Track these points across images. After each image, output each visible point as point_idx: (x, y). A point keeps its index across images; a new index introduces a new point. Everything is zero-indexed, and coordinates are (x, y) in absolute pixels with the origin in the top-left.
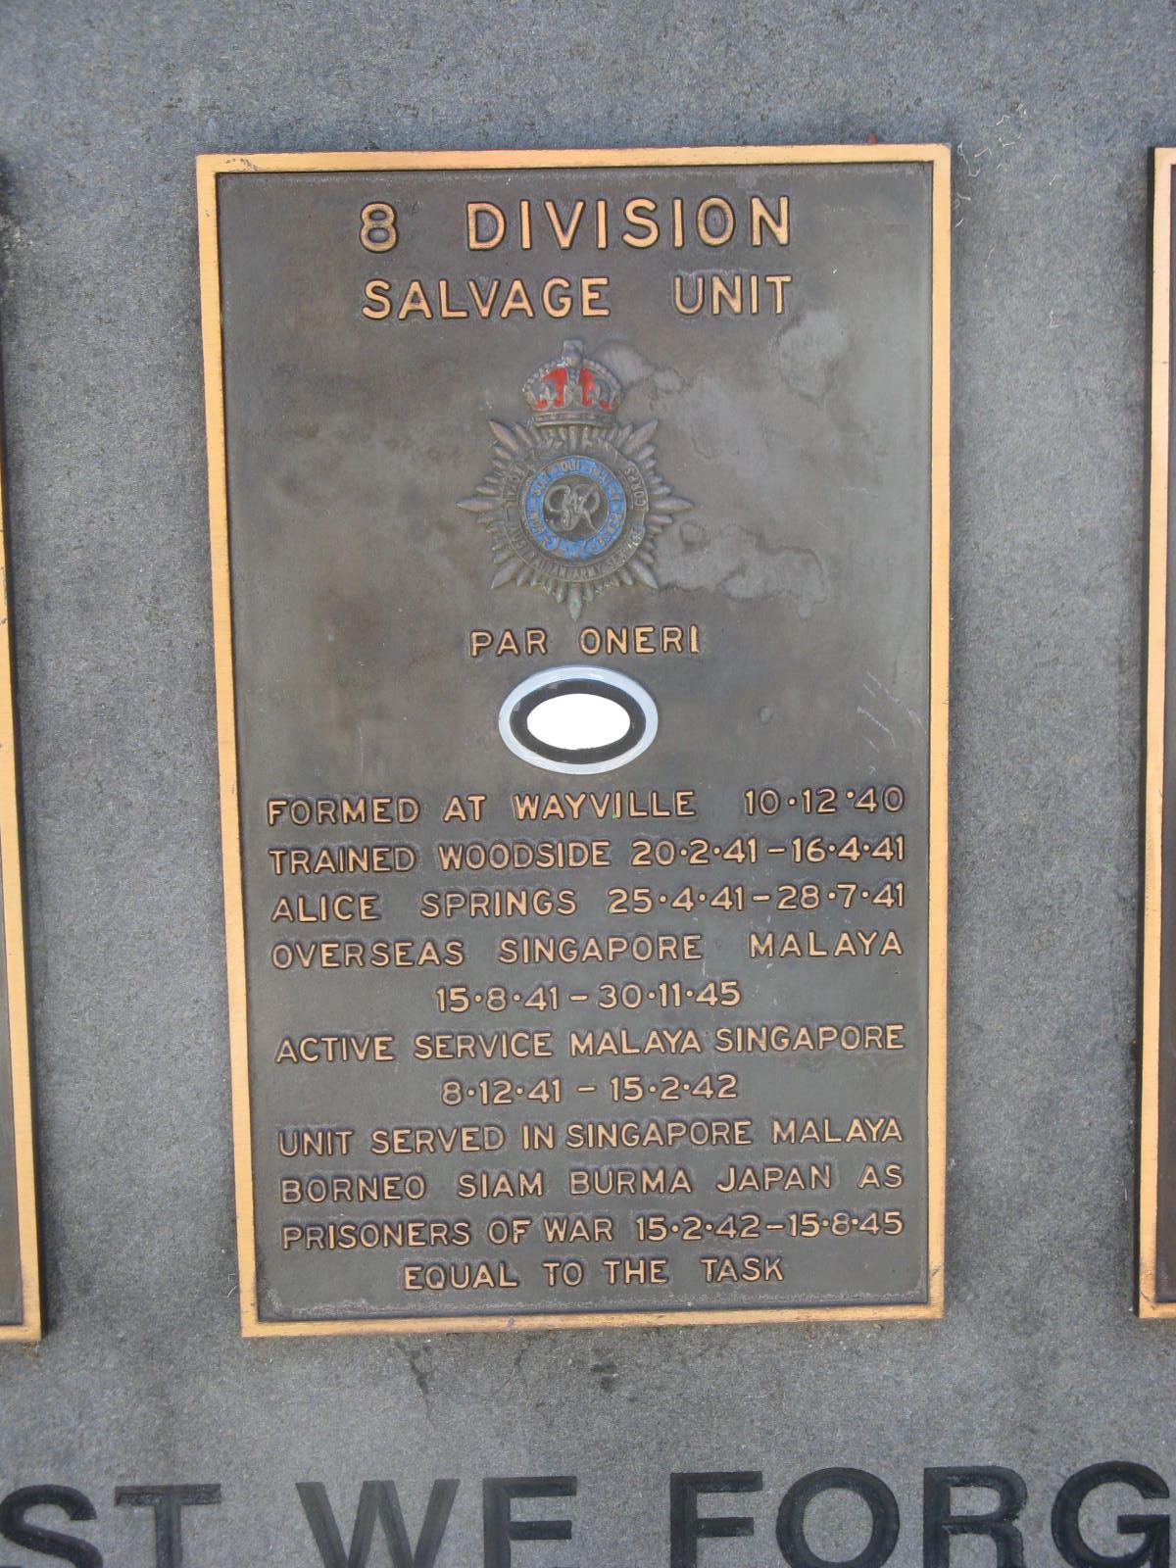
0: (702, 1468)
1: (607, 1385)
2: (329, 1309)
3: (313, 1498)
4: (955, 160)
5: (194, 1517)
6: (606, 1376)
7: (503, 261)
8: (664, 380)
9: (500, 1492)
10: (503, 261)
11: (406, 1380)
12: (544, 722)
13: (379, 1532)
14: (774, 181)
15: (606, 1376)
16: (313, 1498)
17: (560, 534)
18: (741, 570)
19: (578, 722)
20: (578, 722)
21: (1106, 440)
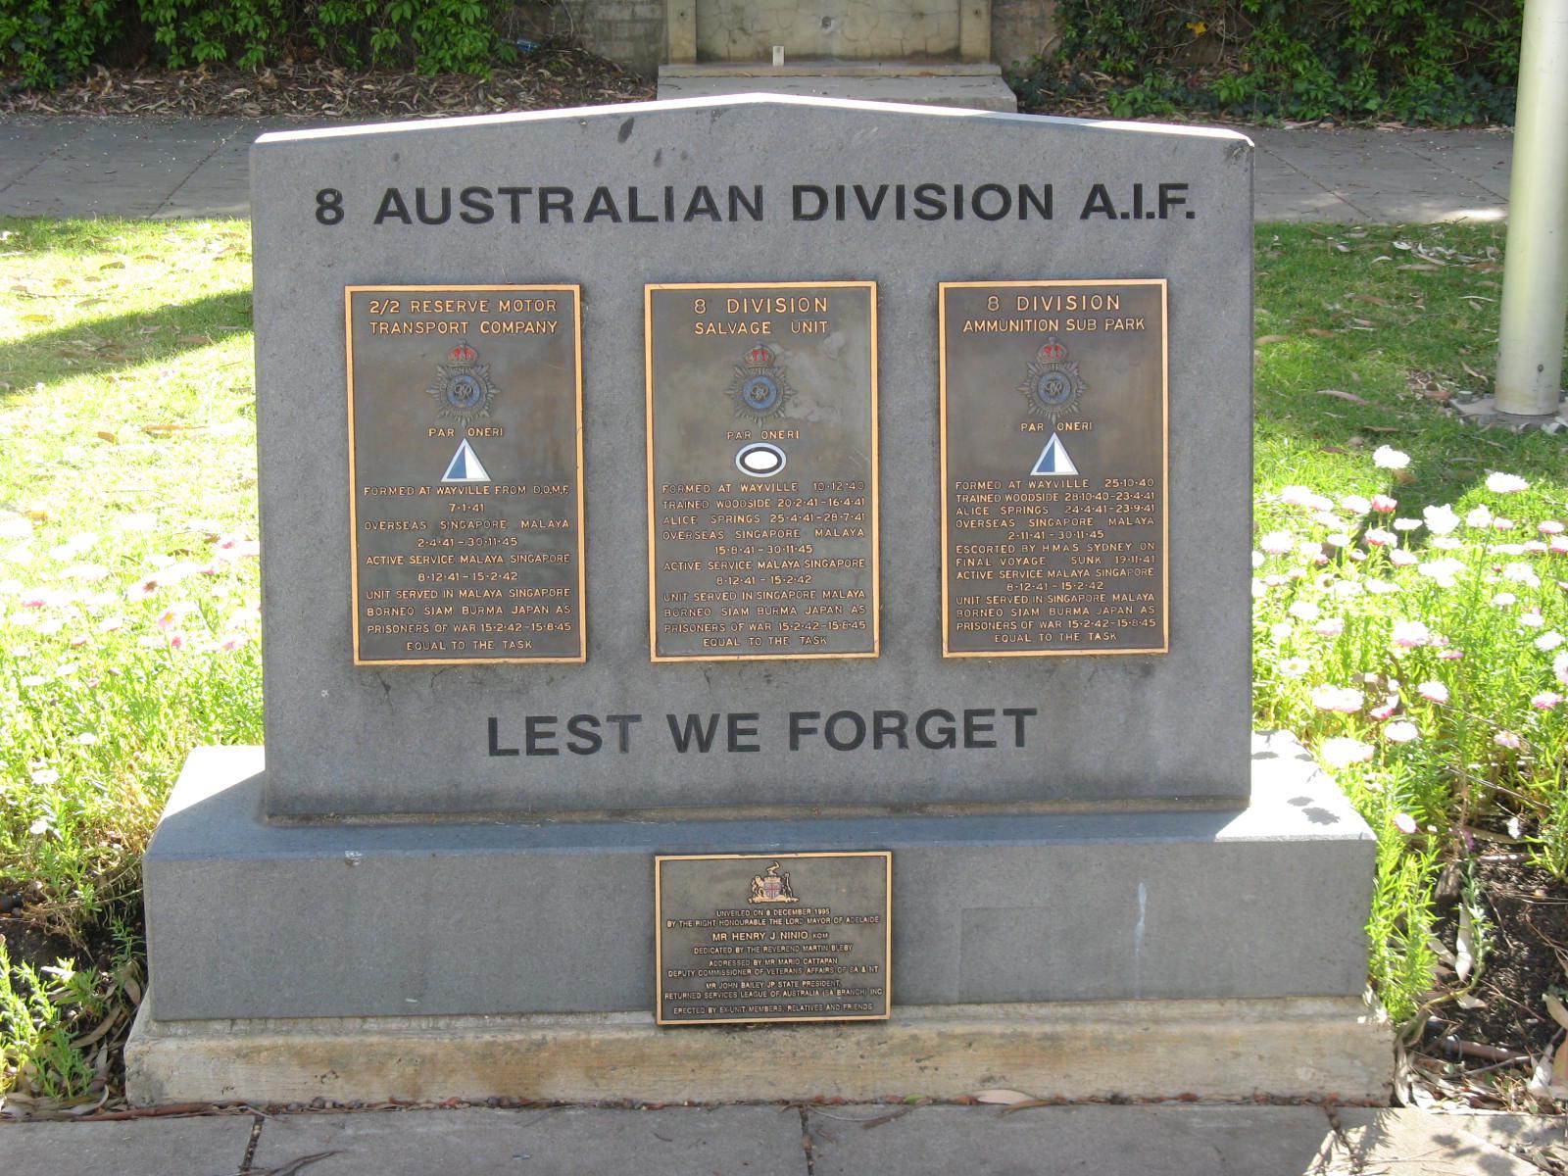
0: (800, 711)
1: (769, 681)
2: (678, 653)
3: (672, 719)
4: (878, 286)
5: (1027, 719)
6: (768, 679)
7: (739, 318)
8: (788, 353)
9: (733, 719)
10: (739, 318)
11: (703, 680)
12: (772, 460)
13: (693, 732)
14: (821, 293)
15: (768, 679)
16: (672, 719)
17: (756, 401)
18: (812, 412)
19: (761, 460)
20: (761, 460)
21: (927, 372)
